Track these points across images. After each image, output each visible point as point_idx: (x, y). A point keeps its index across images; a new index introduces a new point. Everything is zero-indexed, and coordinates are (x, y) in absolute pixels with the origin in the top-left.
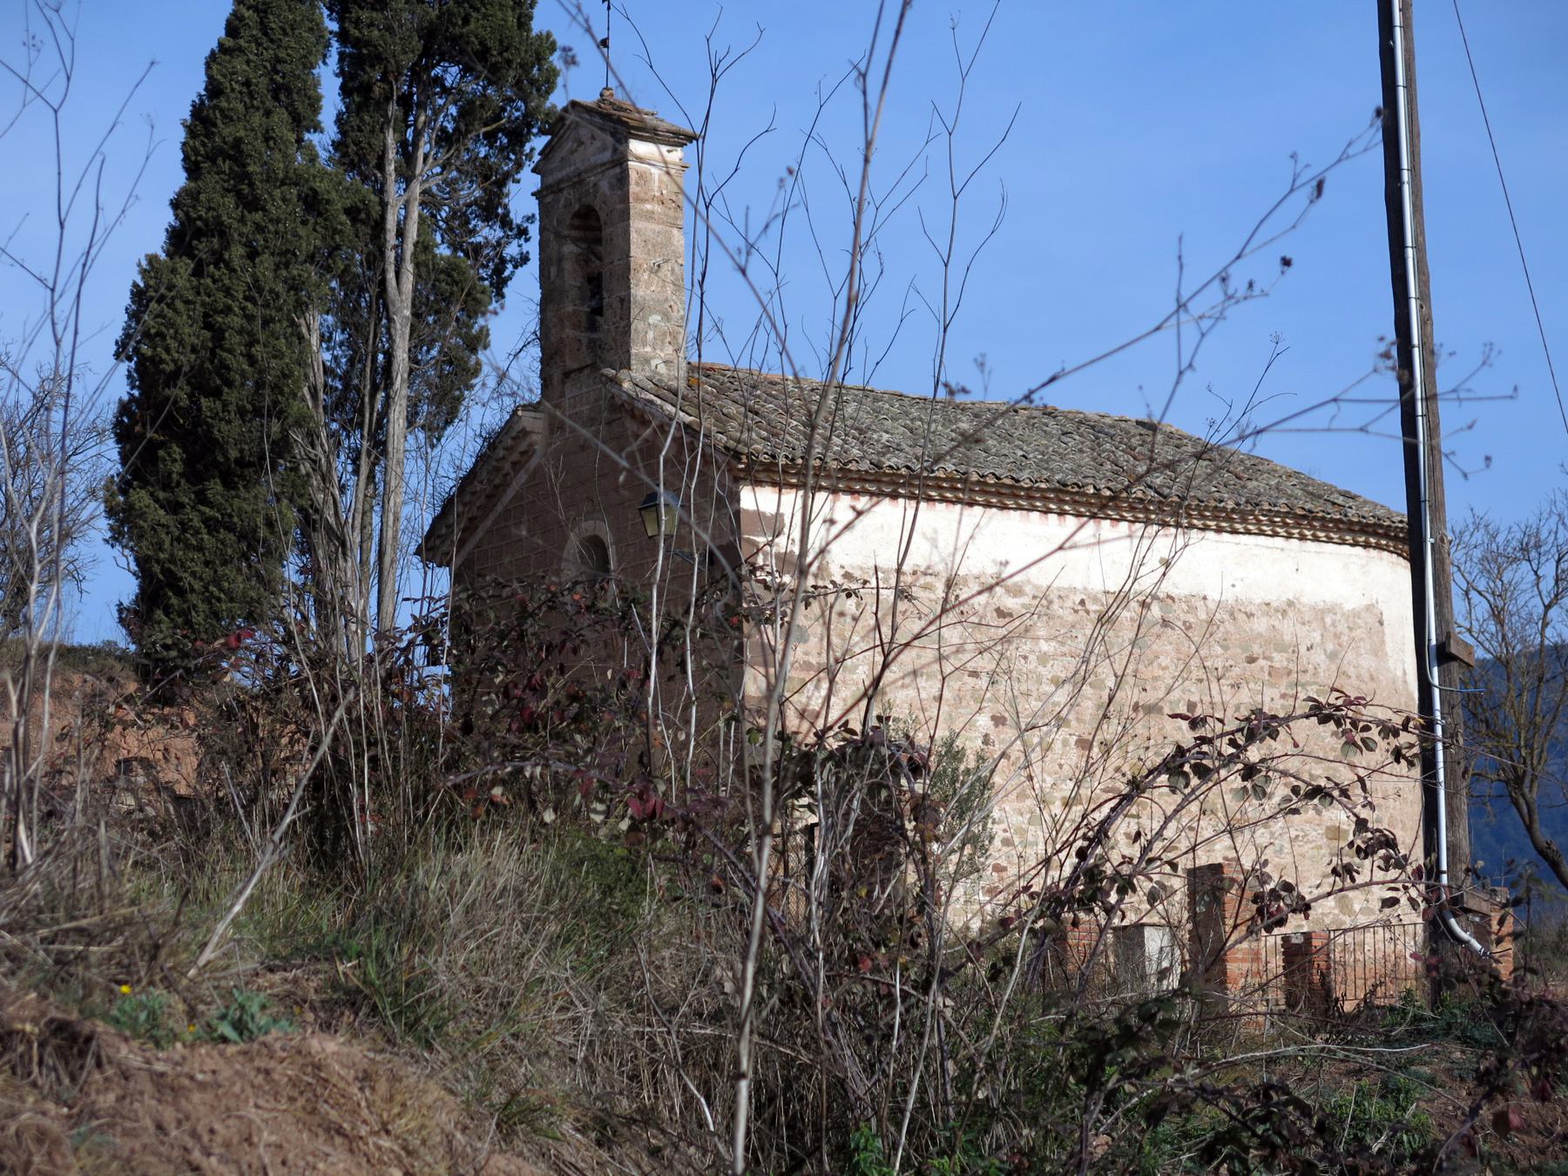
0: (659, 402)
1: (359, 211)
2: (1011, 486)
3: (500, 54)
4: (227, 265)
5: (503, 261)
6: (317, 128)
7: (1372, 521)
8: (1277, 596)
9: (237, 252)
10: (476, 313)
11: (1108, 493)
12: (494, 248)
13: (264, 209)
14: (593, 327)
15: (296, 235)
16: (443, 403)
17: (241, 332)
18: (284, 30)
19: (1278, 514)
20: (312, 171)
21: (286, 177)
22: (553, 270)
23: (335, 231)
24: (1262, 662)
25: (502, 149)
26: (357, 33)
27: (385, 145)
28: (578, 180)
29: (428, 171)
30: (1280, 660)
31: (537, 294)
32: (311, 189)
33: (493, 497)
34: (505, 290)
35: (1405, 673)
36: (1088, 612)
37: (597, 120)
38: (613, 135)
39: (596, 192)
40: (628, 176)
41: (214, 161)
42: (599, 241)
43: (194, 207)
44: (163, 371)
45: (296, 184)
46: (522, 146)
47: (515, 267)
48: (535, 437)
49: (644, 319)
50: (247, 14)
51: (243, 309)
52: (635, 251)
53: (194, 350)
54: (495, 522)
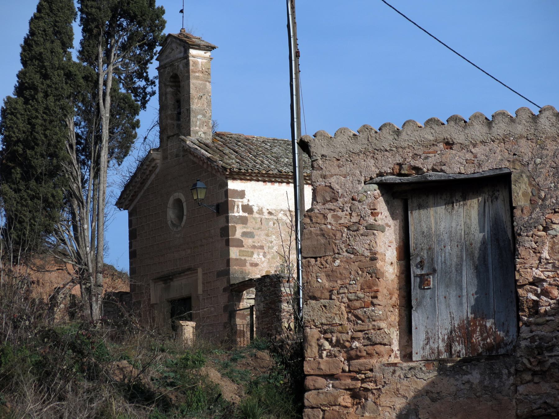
0: (199, 148)
1: (89, 77)
3: (141, 17)
4: (37, 100)
5: (146, 94)
6: (72, 47)
9: (40, 95)
10: (135, 114)
13: (51, 79)
14: (178, 119)
15: (62, 88)
16: (122, 149)
17: (42, 125)
18: (58, 10)
20: (69, 64)
21: (59, 67)
22: (164, 98)
23: (78, 86)
25: (145, 51)
26: (86, 10)
27: (98, 52)
28: (171, 64)
29: (116, 60)
31: (158, 107)
32: (69, 70)
33: (143, 183)
34: (147, 105)
37: (178, 41)
38: (184, 47)
39: (178, 69)
41: (32, 61)
42: (180, 87)
43: (24, 79)
44: (13, 140)
46: (153, 50)
47: (151, 96)
48: (158, 161)
49: (196, 117)
51: (42, 117)
52: (192, 91)
53: (24, 132)
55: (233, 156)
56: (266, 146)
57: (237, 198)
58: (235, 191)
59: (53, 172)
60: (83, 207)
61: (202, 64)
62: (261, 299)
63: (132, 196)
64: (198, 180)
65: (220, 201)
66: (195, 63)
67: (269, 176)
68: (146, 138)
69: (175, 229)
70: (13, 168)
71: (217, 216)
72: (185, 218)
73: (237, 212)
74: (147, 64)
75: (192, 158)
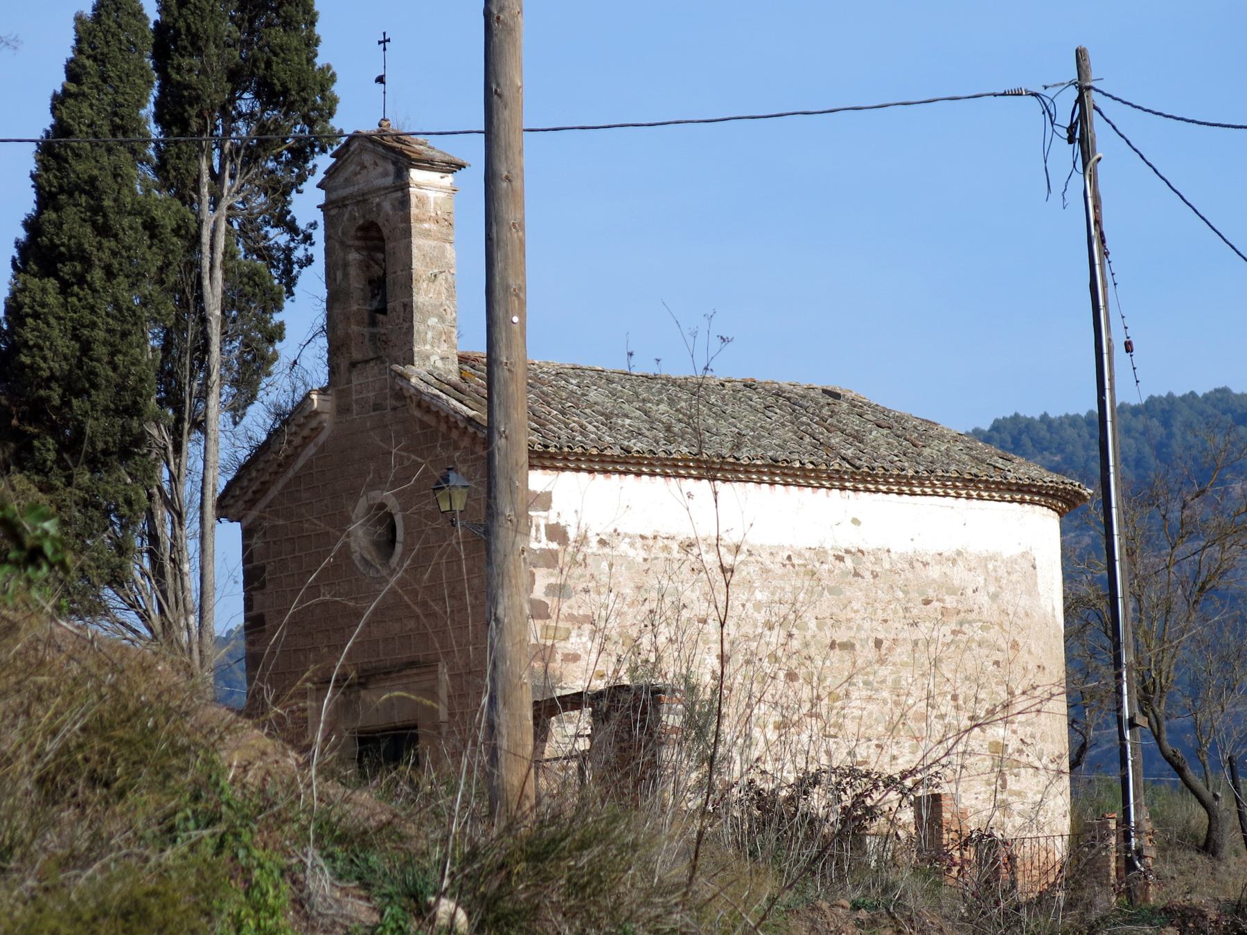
0: (444, 396)
2: (733, 464)
7: (1028, 482)
8: (948, 549)
9: (97, 275)
11: (811, 467)
12: (284, 251)
13: (116, 236)
14: (373, 323)
15: (144, 259)
16: (246, 383)
19: (949, 479)
21: (133, 208)
22: (339, 275)
24: (935, 604)
26: (178, 78)
27: (200, 171)
28: (362, 199)
30: (950, 602)
31: (323, 292)
35: (1054, 609)
36: (793, 566)
37: (380, 149)
38: (394, 163)
40: (409, 200)
41: (71, 195)
43: (57, 235)
45: (140, 214)
46: (306, 161)
47: (301, 267)
48: (325, 417)
49: (424, 321)
50: (88, 63)
52: (417, 265)
53: (66, 358)
54: (286, 486)
59: (129, 448)
60: (181, 524)
61: (436, 203)
63: (254, 492)
64: (449, 469)
66: (422, 201)
67: (602, 459)
68: (295, 362)
70: (37, 436)
72: (399, 548)
73: (539, 542)
74: (289, 194)
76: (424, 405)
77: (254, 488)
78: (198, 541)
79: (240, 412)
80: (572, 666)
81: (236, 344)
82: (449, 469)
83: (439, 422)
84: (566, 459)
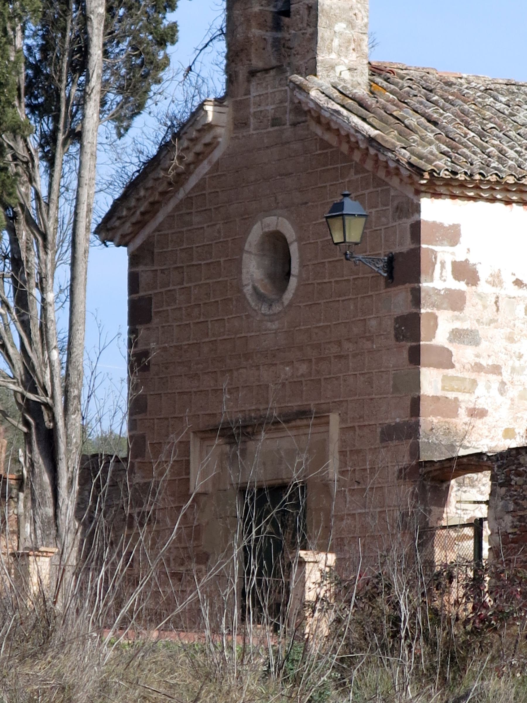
0: (345, 112)
14: (277, 27)
48: (219, 131)
49: (330, 26)
54: (177, 208)
55: (431, 136)
56: (499, 106)
57: (442, 245)
58: (437, 226)
60: (45, 247)
62: (505, 506)
63: (143, 214)
64: (345, 195)
65: (397, 250)
68: (190, 69)
69: (264, 309)
71: (387, 286)
72: (293, 282)
73: (437, 280)
75: (319, 131)
76: (323, 120)
77: (142, 209)
78: (68, 268)
79: (125, 124)
80: (478, 422)
81: (123, 45)
82: (345, 195)
83: (340, 142)
84: (477, 187)
